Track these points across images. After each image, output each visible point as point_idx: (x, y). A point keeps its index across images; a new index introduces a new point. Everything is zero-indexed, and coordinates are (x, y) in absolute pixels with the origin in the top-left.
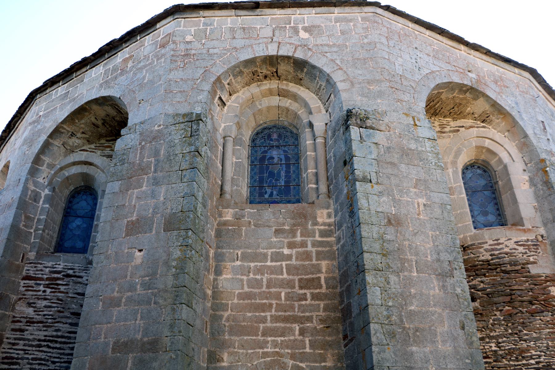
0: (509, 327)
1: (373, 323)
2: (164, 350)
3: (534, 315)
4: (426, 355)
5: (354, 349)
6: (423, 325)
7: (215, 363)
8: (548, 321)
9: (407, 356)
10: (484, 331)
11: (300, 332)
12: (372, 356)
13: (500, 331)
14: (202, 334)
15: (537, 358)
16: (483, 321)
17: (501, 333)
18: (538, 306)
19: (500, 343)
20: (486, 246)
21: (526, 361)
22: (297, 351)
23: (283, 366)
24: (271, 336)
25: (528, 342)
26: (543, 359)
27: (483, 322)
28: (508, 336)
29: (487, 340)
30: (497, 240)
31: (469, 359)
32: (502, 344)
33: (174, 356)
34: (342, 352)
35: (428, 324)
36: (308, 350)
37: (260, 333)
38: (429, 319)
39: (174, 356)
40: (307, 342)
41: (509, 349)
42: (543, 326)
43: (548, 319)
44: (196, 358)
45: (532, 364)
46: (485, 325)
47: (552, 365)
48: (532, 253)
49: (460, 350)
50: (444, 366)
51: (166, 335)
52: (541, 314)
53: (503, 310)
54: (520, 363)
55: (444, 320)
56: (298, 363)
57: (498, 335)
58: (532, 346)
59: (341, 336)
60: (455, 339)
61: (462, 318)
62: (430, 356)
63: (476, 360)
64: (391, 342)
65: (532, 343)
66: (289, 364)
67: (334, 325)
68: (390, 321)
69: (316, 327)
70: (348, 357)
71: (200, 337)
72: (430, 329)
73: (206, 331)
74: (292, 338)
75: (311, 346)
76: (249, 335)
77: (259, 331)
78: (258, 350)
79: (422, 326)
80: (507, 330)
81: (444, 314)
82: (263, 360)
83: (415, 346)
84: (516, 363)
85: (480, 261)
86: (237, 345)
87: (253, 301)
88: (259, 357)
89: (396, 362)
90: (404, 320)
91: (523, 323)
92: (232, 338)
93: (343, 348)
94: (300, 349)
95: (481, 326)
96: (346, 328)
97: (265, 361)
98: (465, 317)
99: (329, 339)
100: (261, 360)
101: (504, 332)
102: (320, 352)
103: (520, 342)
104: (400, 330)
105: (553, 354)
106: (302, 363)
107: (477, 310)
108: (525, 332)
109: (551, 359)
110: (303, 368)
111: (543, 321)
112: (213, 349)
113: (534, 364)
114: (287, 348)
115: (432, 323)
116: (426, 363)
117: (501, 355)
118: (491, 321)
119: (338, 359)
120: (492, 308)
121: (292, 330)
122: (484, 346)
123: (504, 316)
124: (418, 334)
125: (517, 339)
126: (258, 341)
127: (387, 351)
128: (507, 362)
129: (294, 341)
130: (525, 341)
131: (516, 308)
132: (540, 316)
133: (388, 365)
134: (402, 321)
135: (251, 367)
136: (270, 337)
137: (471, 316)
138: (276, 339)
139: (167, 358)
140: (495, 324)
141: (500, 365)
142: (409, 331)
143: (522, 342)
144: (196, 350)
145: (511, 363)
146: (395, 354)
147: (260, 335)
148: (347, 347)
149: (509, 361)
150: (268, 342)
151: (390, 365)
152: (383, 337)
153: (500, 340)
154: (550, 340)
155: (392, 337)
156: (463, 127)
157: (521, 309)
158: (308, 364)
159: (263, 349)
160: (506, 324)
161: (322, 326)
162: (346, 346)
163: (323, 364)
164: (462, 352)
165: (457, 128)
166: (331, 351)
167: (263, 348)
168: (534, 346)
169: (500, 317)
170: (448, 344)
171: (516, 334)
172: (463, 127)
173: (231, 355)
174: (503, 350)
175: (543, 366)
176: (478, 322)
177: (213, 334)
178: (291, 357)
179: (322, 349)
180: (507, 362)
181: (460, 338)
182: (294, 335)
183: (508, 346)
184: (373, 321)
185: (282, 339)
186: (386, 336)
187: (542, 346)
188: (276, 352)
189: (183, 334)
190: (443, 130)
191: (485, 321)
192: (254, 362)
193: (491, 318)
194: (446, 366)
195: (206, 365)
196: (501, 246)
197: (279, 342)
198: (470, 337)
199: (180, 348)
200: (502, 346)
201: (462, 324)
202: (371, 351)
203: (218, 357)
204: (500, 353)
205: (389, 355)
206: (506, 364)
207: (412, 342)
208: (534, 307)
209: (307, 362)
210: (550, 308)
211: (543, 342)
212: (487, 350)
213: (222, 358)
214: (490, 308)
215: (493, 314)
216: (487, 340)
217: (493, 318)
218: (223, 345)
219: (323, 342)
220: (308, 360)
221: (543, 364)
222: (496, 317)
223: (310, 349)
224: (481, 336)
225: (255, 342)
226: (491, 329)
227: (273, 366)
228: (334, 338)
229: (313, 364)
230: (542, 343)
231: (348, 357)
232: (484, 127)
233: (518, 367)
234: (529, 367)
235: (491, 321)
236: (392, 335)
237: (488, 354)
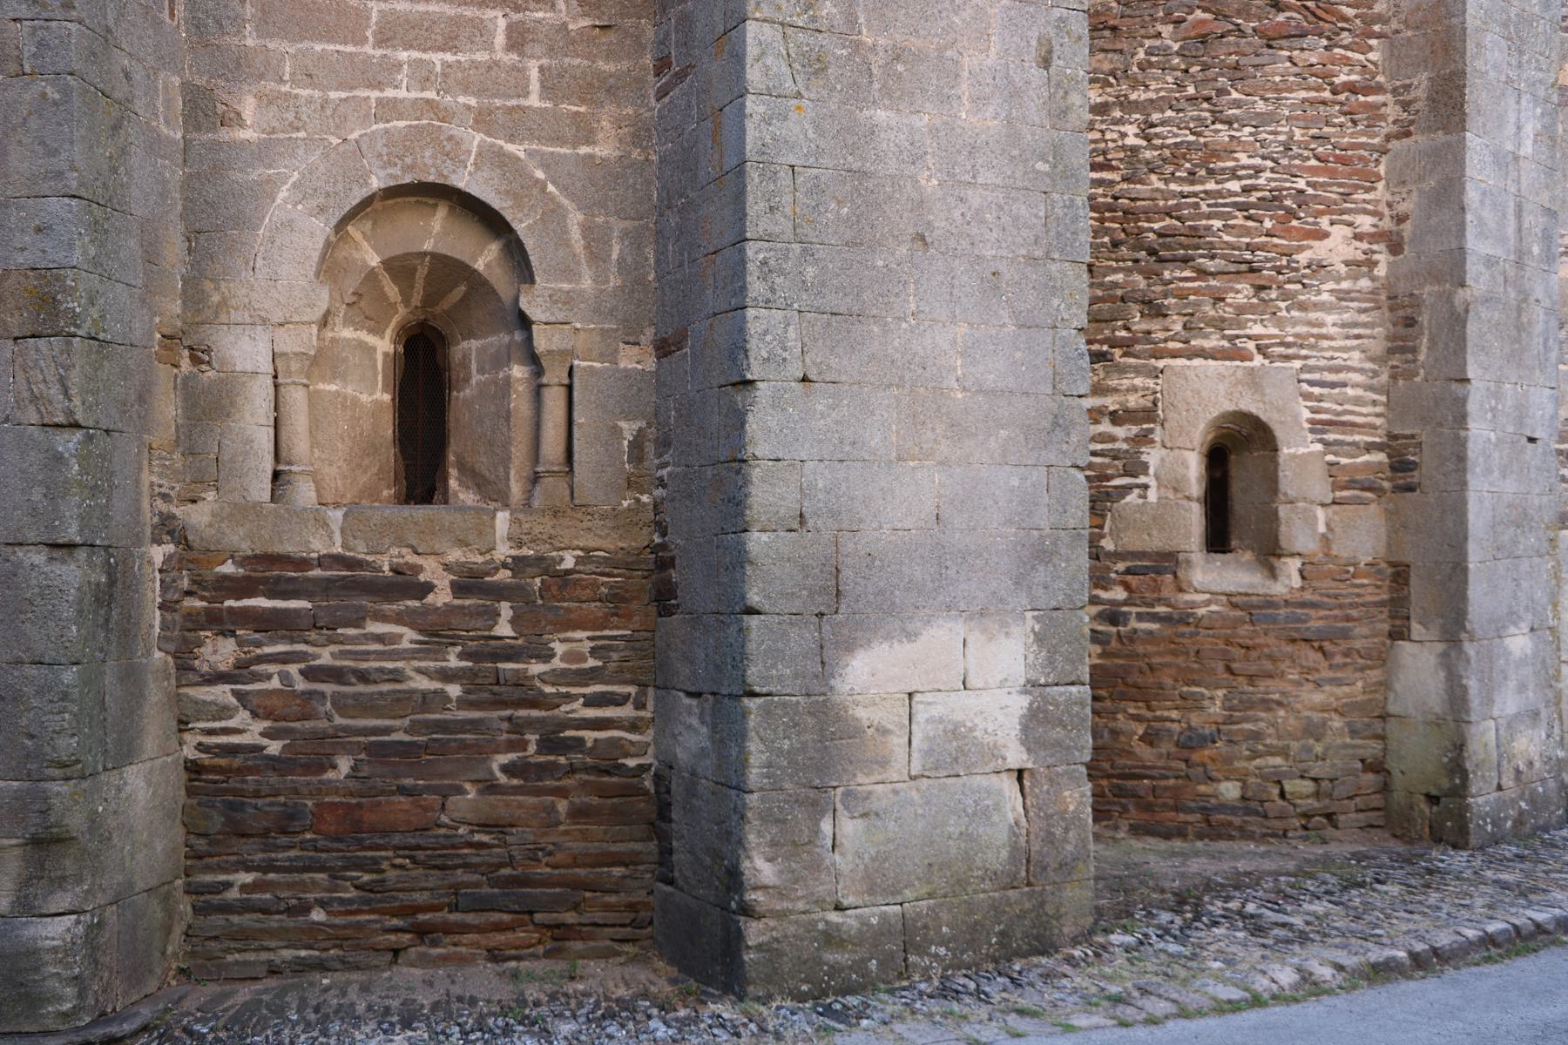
0: (1193, 76)
1: (757, 20)
2: (13, 67)
3: (1273, 43)
4: (917, 138)
5: (689, 106)
6: (919, 43)
7: (213, 129)
8: (1312, 65)
9: (856, 138)
10: (1111, 85)
11: (509, 37)
12: (743, 130)
13: (1161, 89)
14: (157, 24)
15: (1250, 177)
16: (1115, 51)
17: (1162, 94)
18: (1295, 15)
19: (1153, 126)
21: (1217, 183)
22: (498, 102)
23: (448, 148)
24: (408, 46)
25: (1236, 126)
26: (1267, 179)
27: (1116, 57)
28: (1183, 104)
29: (1117, 114)
31: (1048, 162)
32: (1158, 130)
33: (53, 94)
34: (648, 114)
35: (936, 40)
36: (534, 101)
37: (369, 33)
38: (943, 24)
39: (53, 94)
40: (534, 74)
41: (1176, 144)
42: (1292, 79)
43: (1314, 60)
44: (139, 105)
45: (1232, 194)
46: (1119, 65)
47: (1286, 197)
49: (1025, 130)
50: (968, 178)
51: (12, 15)
52: (1296, 42)
53: (1184, 20)
54: (1198, 188)
55: (990, 31)
56: (501, 143)
57: (1152, 101)
58: (1243, 139)
59: (648, 61)
60: (1014, 94)
61: (1049, 28)
62: (928, 142)
63: (1066, 167)
64: (808, 89)
65: (1248, 130)
66: (471, 143)
67: (628, 22)
68: (814, 19)
69: (565, 25)
70: (666, 130)
71: (150, 32)
72: (940, 57)
73: (172, 15)
74: (482, 57)
75: (547, 90)
76: (330, 40)
77: (368, 26)
78: (362, 93)
79: (915, 43)
80: (1180, 86)
81: (992, 11)
82: (381, 126)
83: (886, 108)
84: (1187, 189)
86: (288, 69)
88: (367, 116)
89: (819, 152)
90: (862, 20)
91: (1237, 67)
92: (271, 46)
93: (653, 100)
94: (510, 97)
95: (1106, 67)
96: (667, 34)
97: (387, 131)
98: (1058, 27)
99: (606, 68)
100: (374, 127)
101: (1172, 90)
102: (575, 109)
103: (1213, 127)
104: (844, 52)
105: (1295, 166)
106: (513, 142)
107: (1103, 14)
108: (1235, 95)
109: (1286, 180)
110: (518, 159)
111: (1295, 64)
112: (200, 81)
113: (1236, 194)
114: (466, 91)
115: (950, 38)
116: (913, 163)
117: (1148, 163)
118: (1141, 55)
119: (634, 135)
120: (1152, 12)
121: (481, 31)
122: (1102, 132)
123: (1184, 39)
124: (900, 68)
125: (1207, 114)
126: (364, 62)
127: (793, 116)
128: (1161, 185)
129: (490, 68)
130: (1229, 123)
131: (1225, 16)
132: (1291, 49)
133: (792, 160)
134: (852, 21)
135: (341, 149)
136: (405, 49)
137: (1081, 26)
138: (425, 56)
139: (27, 97)
140: (1151, 65)
141: (1138, 191)
142: (872, 58)
143: (1218, 126)
144: (138, 77)
145: (1173, 186)
146: (817, 127)
147: (371, 39)
148: (666, 100)
149: (1166, 181)
150: (400, 65)
151: (799, 162)
152: (785, 69)
153: (1155, 117)
154: (1301, 124)
155: (816, 73)
157: (1240, 21)
158: (535, 147)
159: (382, 90)
160: (1183, 67)
161: (586, 22)
162: (662, 93)
163: (584, 150)
164: (1029, 137)
166: (613, 107)
167: (379, 86)
168: (1252, 139)
169: (1169, 42)
170: (991, 109)
171: (1208, 99)
173: (270, 103)
174: (1156, 148)
175: (1259, 199)
176: (1101, 56)
177: (198, 27)
178: (476, 121)
179: (583, 101)
180: (1161, 185)
181: (1031, 92)
182: (489, 47)
183: (1176, 135)
184: (758, 15)
185: (449, 57)
186: (797, 66)
187: (1272, 142)
188: (428, 101)
189: (84, 15)
191: (1121, 52)
192: (352, 130)
193: (1142, 46)
194: (974, 177)
195: (179, 135)
197: (438, 68)
198: (1061, 93)
199: (76, 66)
200: (1157, 135)
201: (1044, 49)
202: (741, 114)
203: (221, 108)
204: (1148, 154)
205: (796, 130)
206: (1157, 190)
207: (877, 94)
208: (1281, 18)
209: (531, 141)
210: (1327, 25)
211: (1279, 129)
212: (1111, 145)
213: (239, 114)
214: (1147, 12)
215: (1152, 31)
216: (1117, 114)
217: (1148, 43)
218: (239, 68)
219: (589, 79)
220: (532, 136)
221: (1260, 194)
222: (1157, 43)
223: (542, 98)
224: (1099, 100)
225: (352, 62)
226: (1136, 80)
227: (418, 149)
228: (625, 65)
229: (551, 149)
230: (1275, 133)
231: (666, 130)
233: (1188, 200)
234: (1220, 201)
235: (1141, 55)
236: (816, 65)
237: (1109, 157)
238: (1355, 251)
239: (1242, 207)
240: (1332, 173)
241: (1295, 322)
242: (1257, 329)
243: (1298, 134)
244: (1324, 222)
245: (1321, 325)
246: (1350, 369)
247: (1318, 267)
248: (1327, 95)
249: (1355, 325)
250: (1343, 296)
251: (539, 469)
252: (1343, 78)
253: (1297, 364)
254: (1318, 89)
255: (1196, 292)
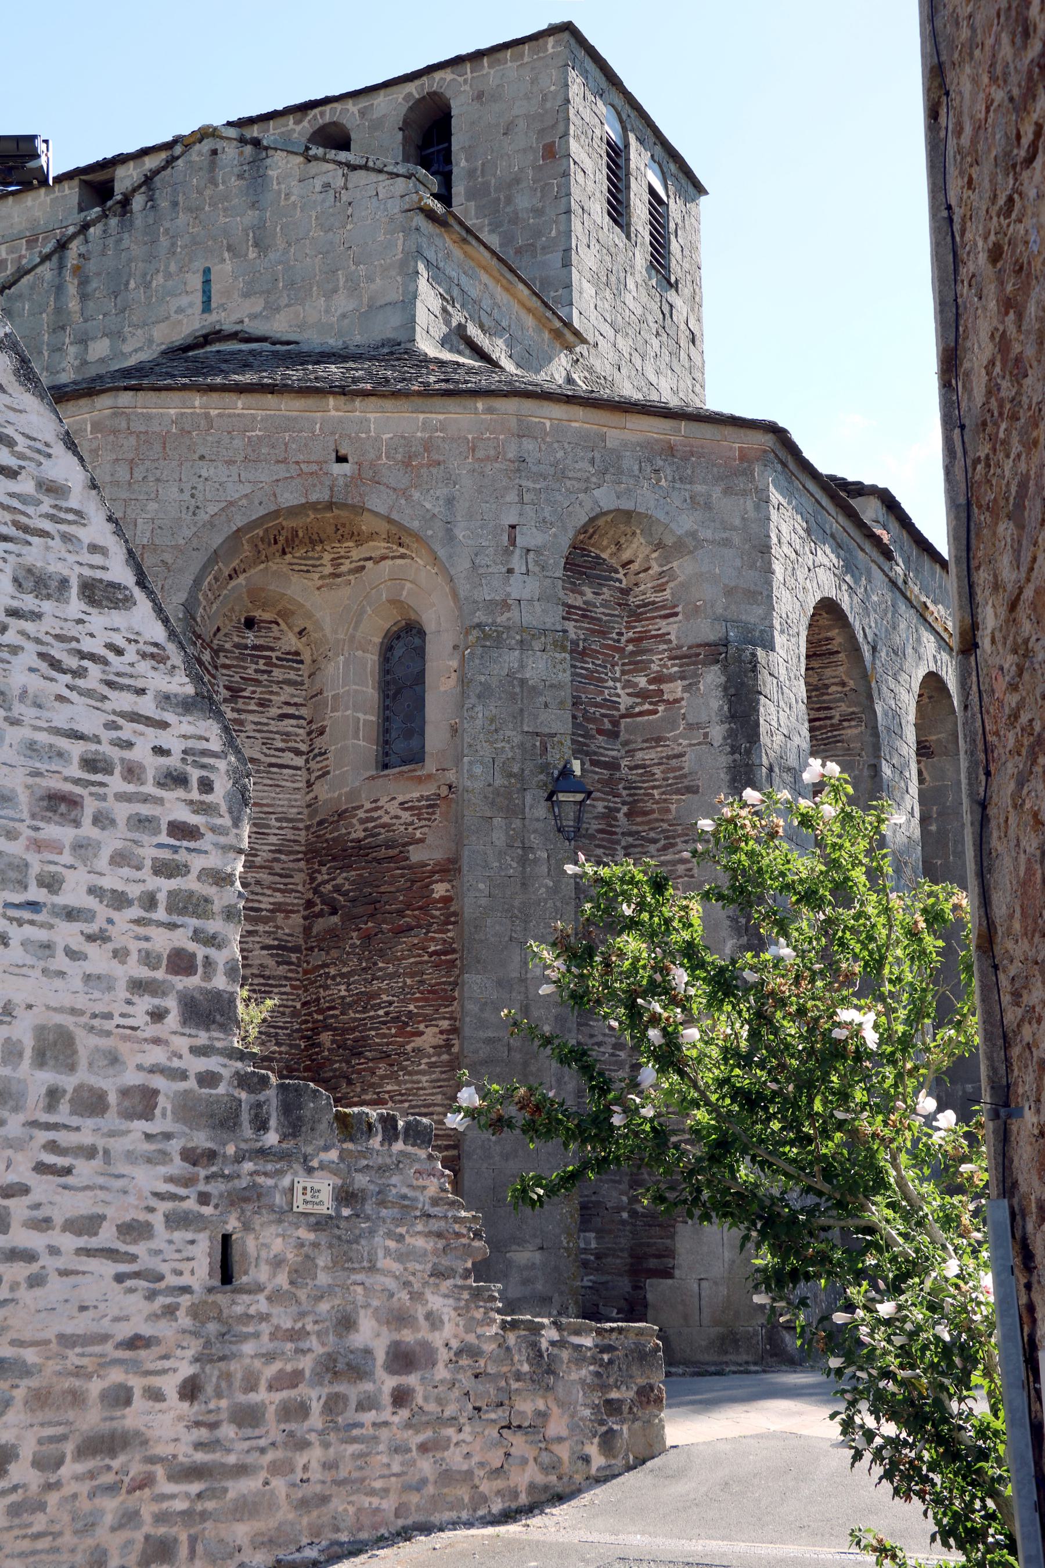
20: (361, 814)
30: (375, 801)
45: (380, 1016)
48: (423, 823)
85: (352, 841)
87: (509, 1319)
108: (381, 965)
156: (370, 559)
165: (362, 563)
172: (370, 559)
190: (338, 571)
196: (380, 813)
232: (402, 556)
238: (440, 1040)
239: (384, 1023)
240: (426, 1000)
241: (405, 1082)
242: (389, 1088)
243: (409, 981)
244: (422, 1027)
245: (419, 1082)
246: (435, 1105)
247: (418, 1050)
248: (426, 958)
249: (438, 1080)
250: (431, 1065)
251: (251, 216)
252: (433, 948)
253: (406, 1105)
254: (420, 956)
255: (364, 1070)
